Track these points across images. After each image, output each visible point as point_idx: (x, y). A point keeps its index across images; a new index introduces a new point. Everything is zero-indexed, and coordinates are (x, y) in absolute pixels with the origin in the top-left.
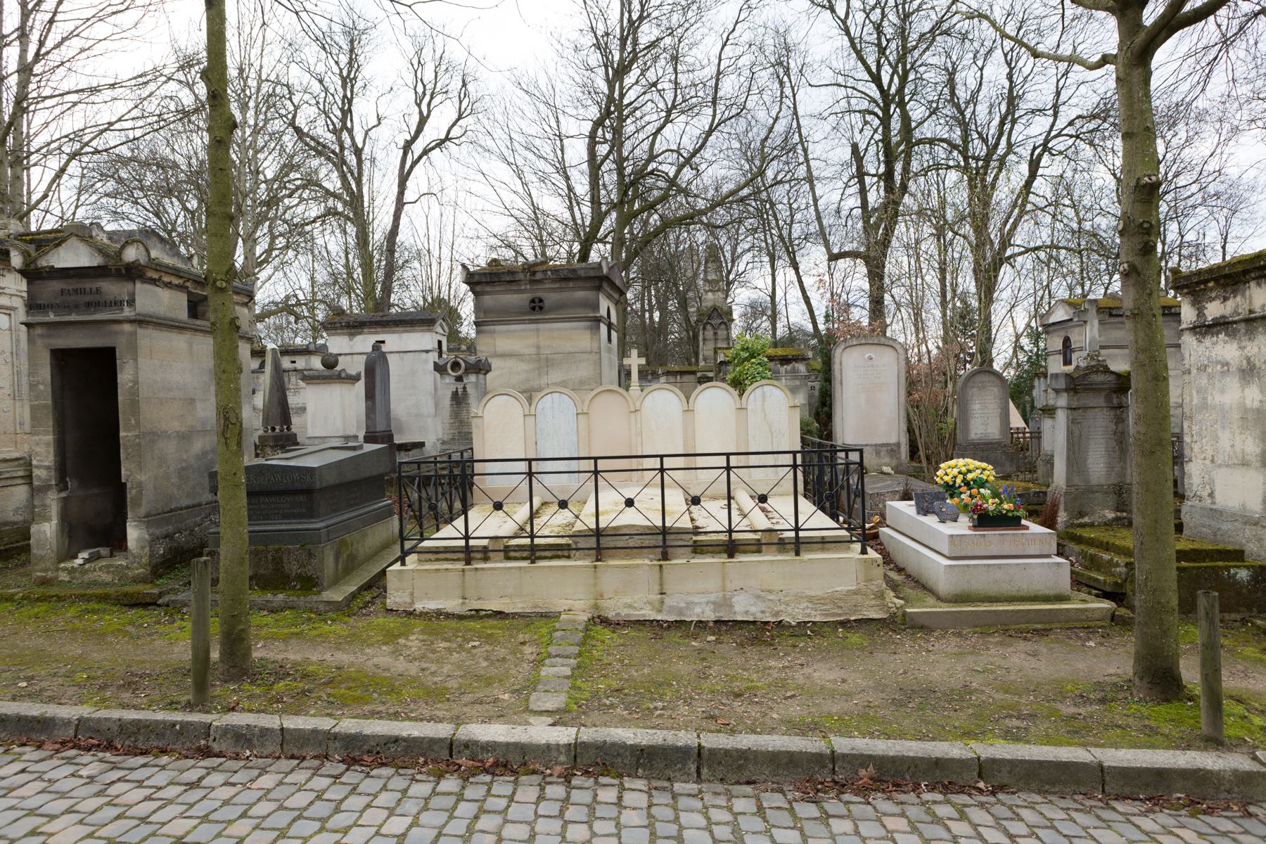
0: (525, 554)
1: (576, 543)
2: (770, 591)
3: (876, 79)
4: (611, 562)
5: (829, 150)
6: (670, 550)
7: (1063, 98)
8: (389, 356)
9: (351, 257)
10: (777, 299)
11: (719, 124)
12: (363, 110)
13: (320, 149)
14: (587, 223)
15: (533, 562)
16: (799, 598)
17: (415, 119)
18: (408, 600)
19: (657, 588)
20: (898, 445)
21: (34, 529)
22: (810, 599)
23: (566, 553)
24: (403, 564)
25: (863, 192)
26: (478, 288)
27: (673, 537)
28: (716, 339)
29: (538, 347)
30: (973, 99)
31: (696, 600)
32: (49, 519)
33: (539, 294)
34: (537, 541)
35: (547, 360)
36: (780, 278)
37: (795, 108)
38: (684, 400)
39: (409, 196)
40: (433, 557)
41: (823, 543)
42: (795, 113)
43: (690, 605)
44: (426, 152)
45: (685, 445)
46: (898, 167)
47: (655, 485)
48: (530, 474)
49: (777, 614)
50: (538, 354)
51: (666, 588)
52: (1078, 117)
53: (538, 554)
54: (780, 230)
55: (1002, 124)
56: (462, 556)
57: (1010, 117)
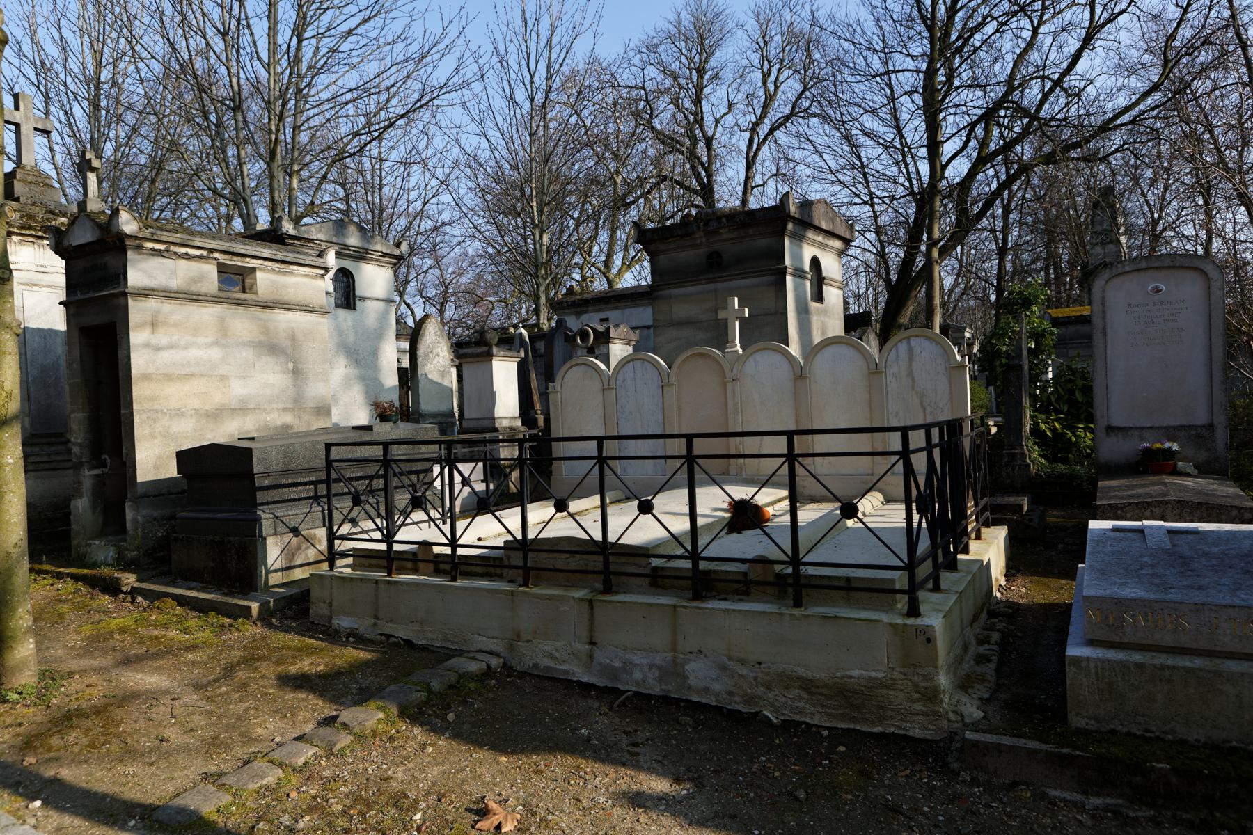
0: (463, 568)
2: (743, 662)
12: (715, 99)
15: (454, 580)
16: (786, 680)
20: (1211, 426)
21: (73, 504)
22: (809, 686)
23: (498, 571)
24: (390, 575)
26: (652, 247)
31: (636, 659)
32: (81, 496)
43: (628, 667)
44: (771, 131)
45: (797, 422)
47: (778, 485)
49: (750, 700)
53: (463, 568)
56: (384, 563)
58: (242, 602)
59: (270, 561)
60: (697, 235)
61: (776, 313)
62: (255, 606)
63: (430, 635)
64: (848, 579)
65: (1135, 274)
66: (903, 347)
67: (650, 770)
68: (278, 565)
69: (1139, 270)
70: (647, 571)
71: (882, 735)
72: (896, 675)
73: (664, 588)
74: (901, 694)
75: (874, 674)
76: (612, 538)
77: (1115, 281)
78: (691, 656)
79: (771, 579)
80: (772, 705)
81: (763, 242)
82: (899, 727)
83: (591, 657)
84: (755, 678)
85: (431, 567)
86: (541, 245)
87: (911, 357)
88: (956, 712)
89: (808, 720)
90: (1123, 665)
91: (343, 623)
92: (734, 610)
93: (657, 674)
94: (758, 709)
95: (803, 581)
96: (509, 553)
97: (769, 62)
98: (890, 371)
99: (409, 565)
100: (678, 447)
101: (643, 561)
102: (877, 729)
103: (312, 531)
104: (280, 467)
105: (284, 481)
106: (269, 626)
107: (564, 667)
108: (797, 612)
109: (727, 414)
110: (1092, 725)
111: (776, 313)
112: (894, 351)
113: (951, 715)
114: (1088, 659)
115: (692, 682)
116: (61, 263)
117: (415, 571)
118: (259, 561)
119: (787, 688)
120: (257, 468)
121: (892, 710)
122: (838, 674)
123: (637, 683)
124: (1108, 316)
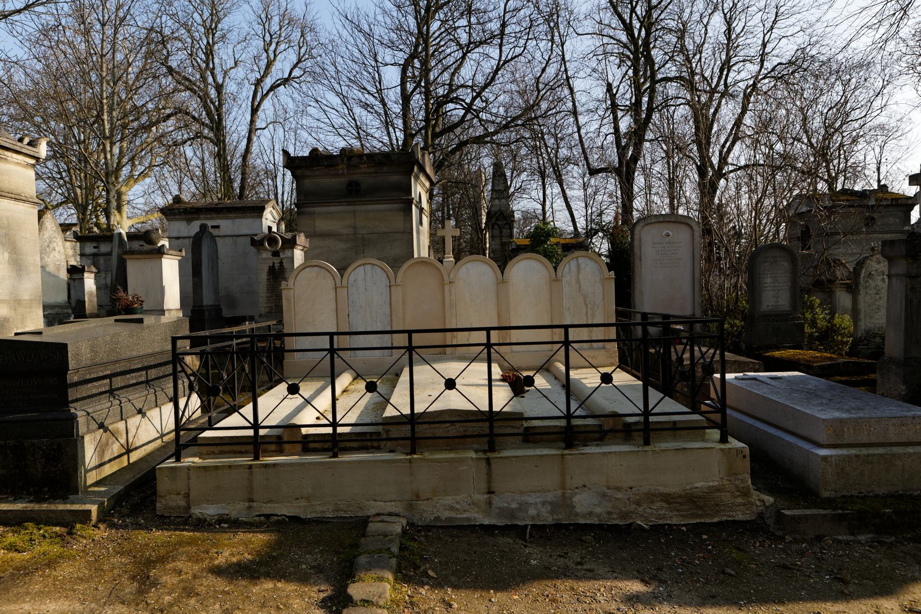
0: (327, 445)
1: (387, 432)
2: (618, 489)
3: (628, 28)
7: (767, 50)
8: (217, 239)
11: (503, 64)
12: (224, 54)
14: (400, 143)
15: (335, 456)
16: (651, 497)
17: (263, 63)
18: (182, 503)
19: (483, 486)
22: (667, 498)
23: (375, 444)
24: (178, 460)
26: (298, 172)
28: (501, 237)
29: (355, 228)
30: (699, 49)
31: (531, 500)
33: (356, 178)
36: (548, 192)
37: (563, 55)
38: (499, 272)
39: (259, 124)
40: (216, 449)
41: (674, 429)
42: (563, 59)
43: (523, 507)
44: (273, 88)
47: (481, 360)
48: (332, 351)
49: (624, 515)
52: (779, 64)
53: (342, 445)
54: (549, 154)
55: (721, 70)
57: (726, 66)
59: (87, 460)
60: (340, 167)
61: (404, 232)
62: (94, 508)
63: (320, 508)
64: (675, 422)
66: (573, 264)
67: (629, 578)
68: (92, 465)
69: (659, 222)
70: (521, 431)
71: (720, 523)
72: (725, 482)
74: (728, 494)
75: (711, 484)
76: (496, 408)
77: (647, 228)
78: (577, 491)
79: (620, 427)
80: (641, 516)
81: (394, 178)
82: (729, 516)
83: (490, 503)
84: (629, 499)
85: (299, 447)
86: (112, 155)
88: (759, 500)
89: (669, 522)
90: (849, 456)
92: (610, 453)
93: (549, 508)
94: (631, 521)
95: (651, 427)
96: (388, 427)
98: (564, 280)
99: (273, 447)
100: (481, 337)
101: (518, 423)
102: (716, 520)
103: (115, 425)
104: (89, 362)
105: (88, 377)
106: (112, 526)
107: (465, 516)
108: (647, 448)
109: (444, 307)
111: (404, 232)
113: (758, 503)
114: (831, 456)
115: (579, 509)
116: (306, 154)
117: (281, 452)
118: (79, 461)
119: (652, 502)
120: (72, 364)
121: (724, 505)
122: (688, 487)
123: (533, 518)
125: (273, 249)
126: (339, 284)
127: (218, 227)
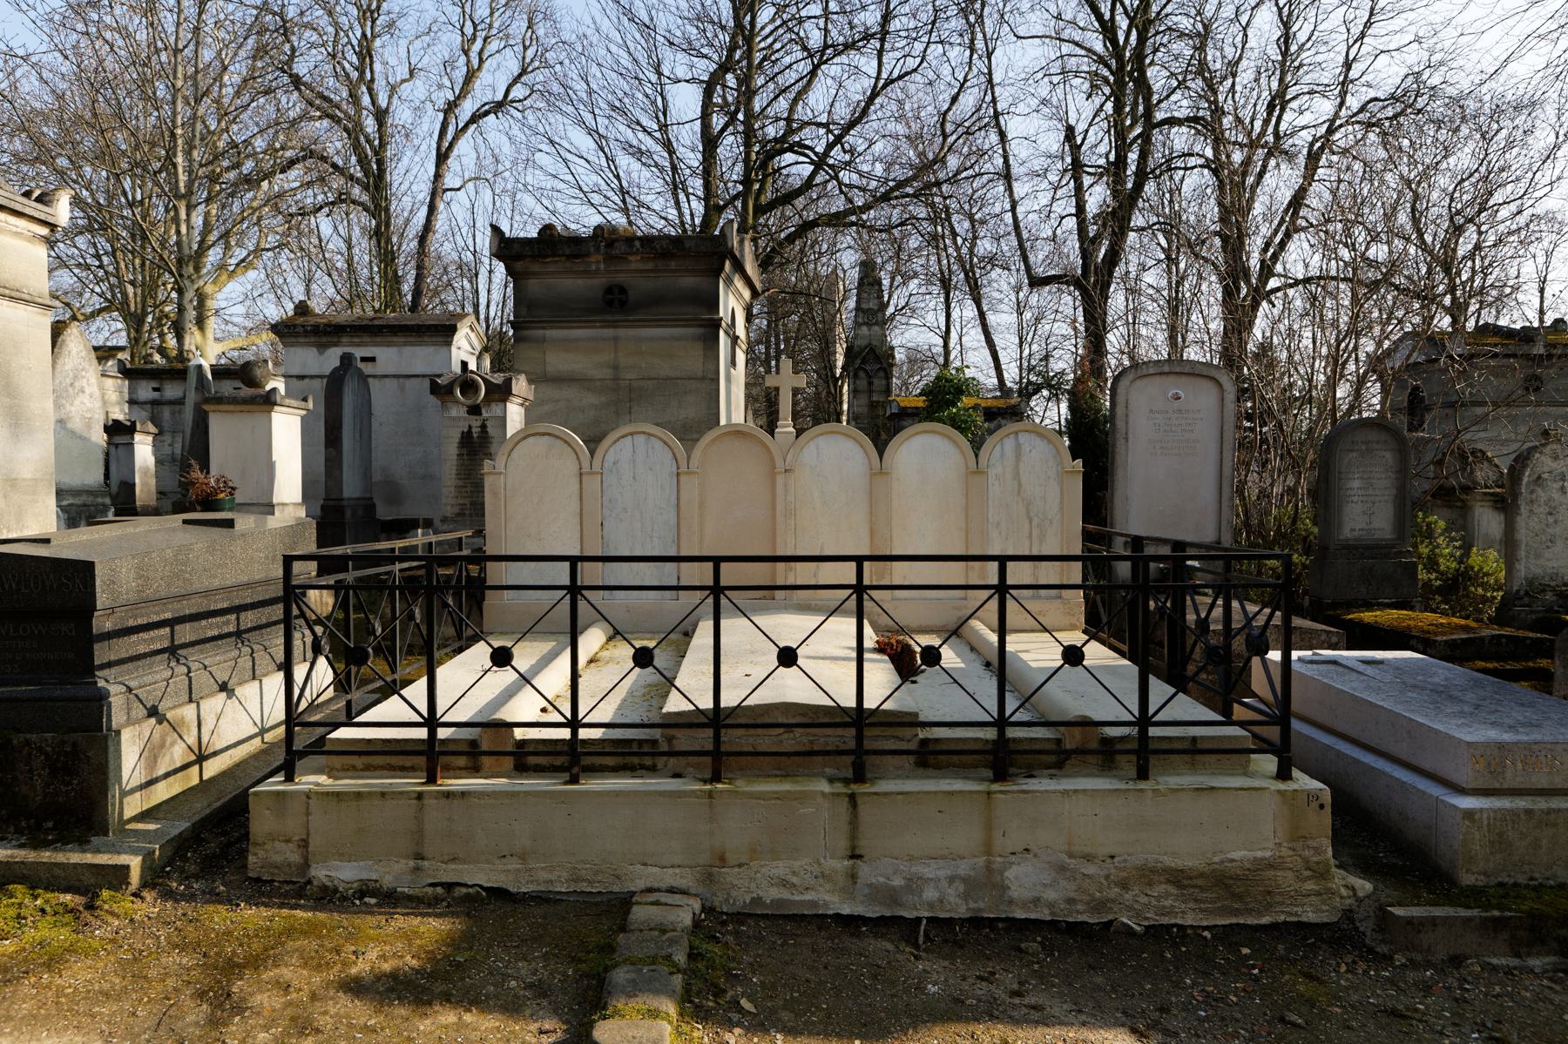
0: (559, 761)
1: (670, 740)
2: (1089, 858)
4: (742, 785)
5: (1032, 136)
6: (870, 760)
7: (1353, 74)
9: (356, 250)
10: (952, 345)
11: (884, 87)
12: (390, 57)
13: (326, 108)
14: (697, 221)
15: (574, 780)
16: (1148, 874)
19: (843, 844)
22: (1178, 878)
23: (648, 761)
24: (289, 778)
25: (1079, 191)
26: (519, 266)
27: (877, 731)
28: (871, 391)
29: (616, 367)
30: (1233, 67)
31: (928, 871)
33: (620, 278)
34: (584, 734)
35: (631, 389)
36: (955, 314)
37: (990, 73)
39: (450, 180)
40: (358, 761)
41: (1194, 751)
42: (990, 81)
43: (914, 884)
44: (475, 118)
46: (1133, 156)
47: (846, 614)
48: (574, 590)
49: (1099, 906)
50: (616, 379)
51: (864, 845)
53: (587, 761)
54: (958, 249)
57: (1278, 102)
58: (103, 859)
60: (592, 259)
61: (703, 378)
62: (135, 863)
63: (544, 875)
64: (1194, 739)
65: (1157, 378)
66: (1009, 443)
70: (913, 746)
71: (1274, 926)
72: (1285, 852)
73: (938, 767)
74: (1290, 874)
75: (1259, 854)
76: (870, 703)
77: (1138, 383)
78: (1013, 859)
80: (1130, 908)
81: (688, 282)
83: (853, 876)
84: (1107, 877)
85: (509, 762)
86: (190, 227)
87: (1018, 457)
88: (1346, 886)
89: (1179, 921)
90: (1514, 813)
91: (345, 873)
92: (1076, 791)
93: (961, 888)
94: (1111, 917)
95: (1152, 746)
97: (475, 26)
98: (992, 473)
99: (462, 761)
101: (908, 732)
102: (1265, 920)
104: (133, 597)
105: (131, 623)
106: (168, 895)
107: (808, 897)
108: (1142, 785)
109: (774, 516)
110: (1481, 881)
111: (703, 378)
112: (998, 447)
113: (1344, 892)
115: (1014, 893)
117: (475, 770)
118: (111, 775)
119: (1150, 884)
120: (102, 599)
121: (1281, 894)
122: (1216, 859)
123: (931, 906)
124: (1131, 417)
125: (469, 402)
126: (586, 468)
127: (373, 359)
